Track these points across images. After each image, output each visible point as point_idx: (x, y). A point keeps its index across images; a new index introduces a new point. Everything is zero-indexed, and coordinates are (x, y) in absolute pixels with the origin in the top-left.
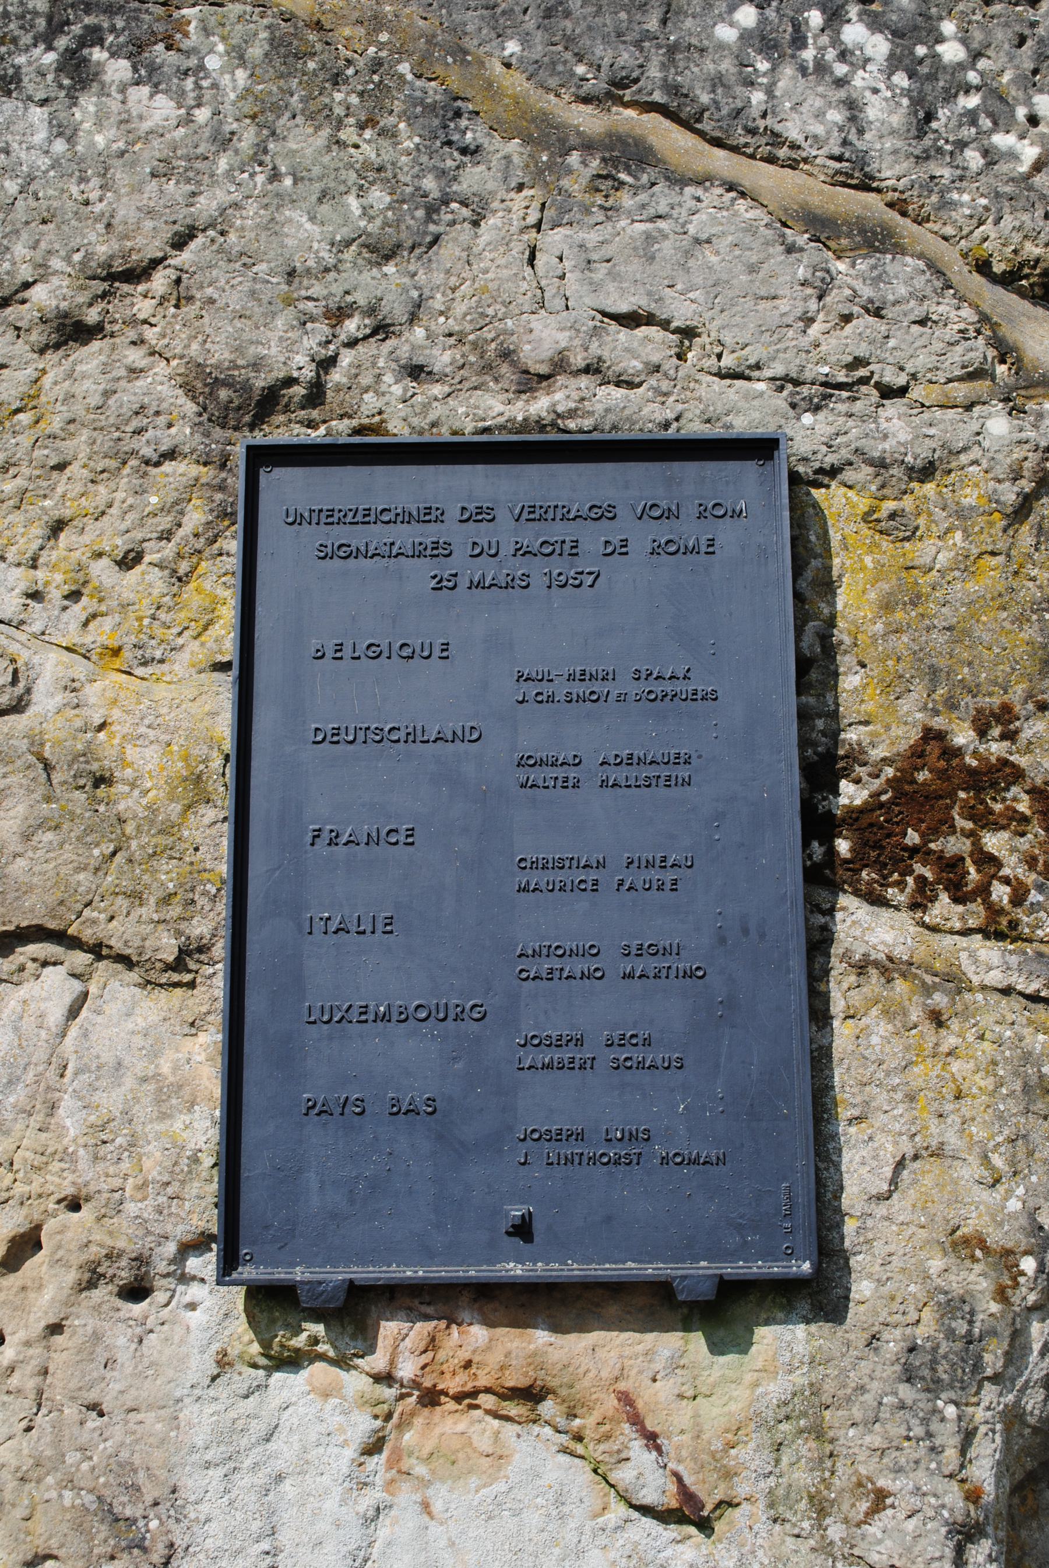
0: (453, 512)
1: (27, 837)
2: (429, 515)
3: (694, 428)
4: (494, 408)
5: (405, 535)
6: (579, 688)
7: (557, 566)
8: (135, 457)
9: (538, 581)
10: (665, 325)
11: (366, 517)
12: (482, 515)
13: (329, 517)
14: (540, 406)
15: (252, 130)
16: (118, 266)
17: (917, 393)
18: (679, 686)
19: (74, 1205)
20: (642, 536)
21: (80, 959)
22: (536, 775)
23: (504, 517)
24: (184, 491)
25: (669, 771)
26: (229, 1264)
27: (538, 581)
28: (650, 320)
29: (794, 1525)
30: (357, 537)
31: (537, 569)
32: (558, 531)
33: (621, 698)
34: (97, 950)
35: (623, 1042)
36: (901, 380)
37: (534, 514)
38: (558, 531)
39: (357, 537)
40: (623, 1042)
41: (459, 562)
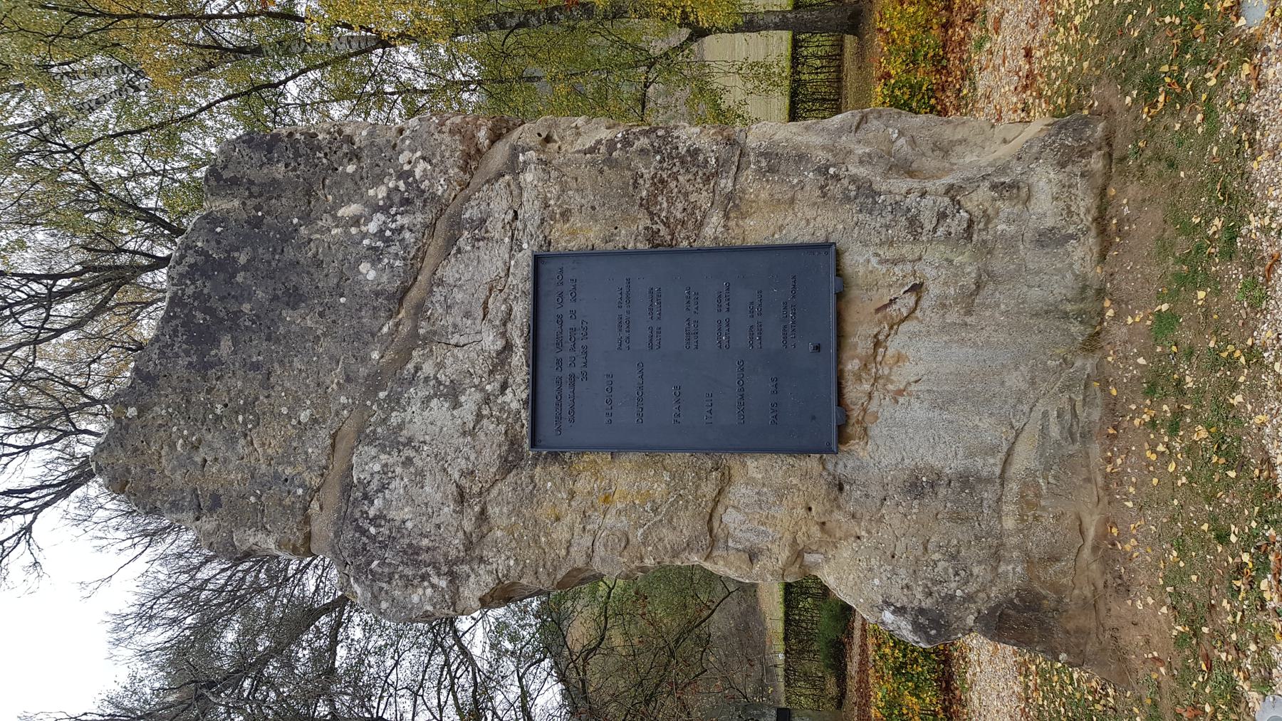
0: (558, 374)
1: (675, 528)
2: (559, 381)
3: (529, 286)
4: (518, 358)
5: (566, 390)
6: (625, 326)
7: (578, 335)
8: (532, 496)
9: (584, 343)
10: (488, 298)
11: (559, 404)
12: (559, 362)
13: (559, 418)
14: (518, 342)
15: (739, 83)
16: (459, 499)
17: (516, 207)
18: (625, 291)
19: (810, 509)
20: (569, 306)
21: (720, 509)
22: (655, 343)
23: (560, 355)
24: (547, 477)
25: (655, 296)
26: (830, 451)
27: (584, 343)
28: (486, 303)
29: (1195, 415)
30: (566, 408)
31: (579, 344)
32: (566, 334)
33: (628, 312)
34: (716, 503)
35: (752, 311)
36: (511, 212)
37: (559, 344)
38: (566, 334)
39: (566, 408)
40: (752, 311)
41: (577, 371)
